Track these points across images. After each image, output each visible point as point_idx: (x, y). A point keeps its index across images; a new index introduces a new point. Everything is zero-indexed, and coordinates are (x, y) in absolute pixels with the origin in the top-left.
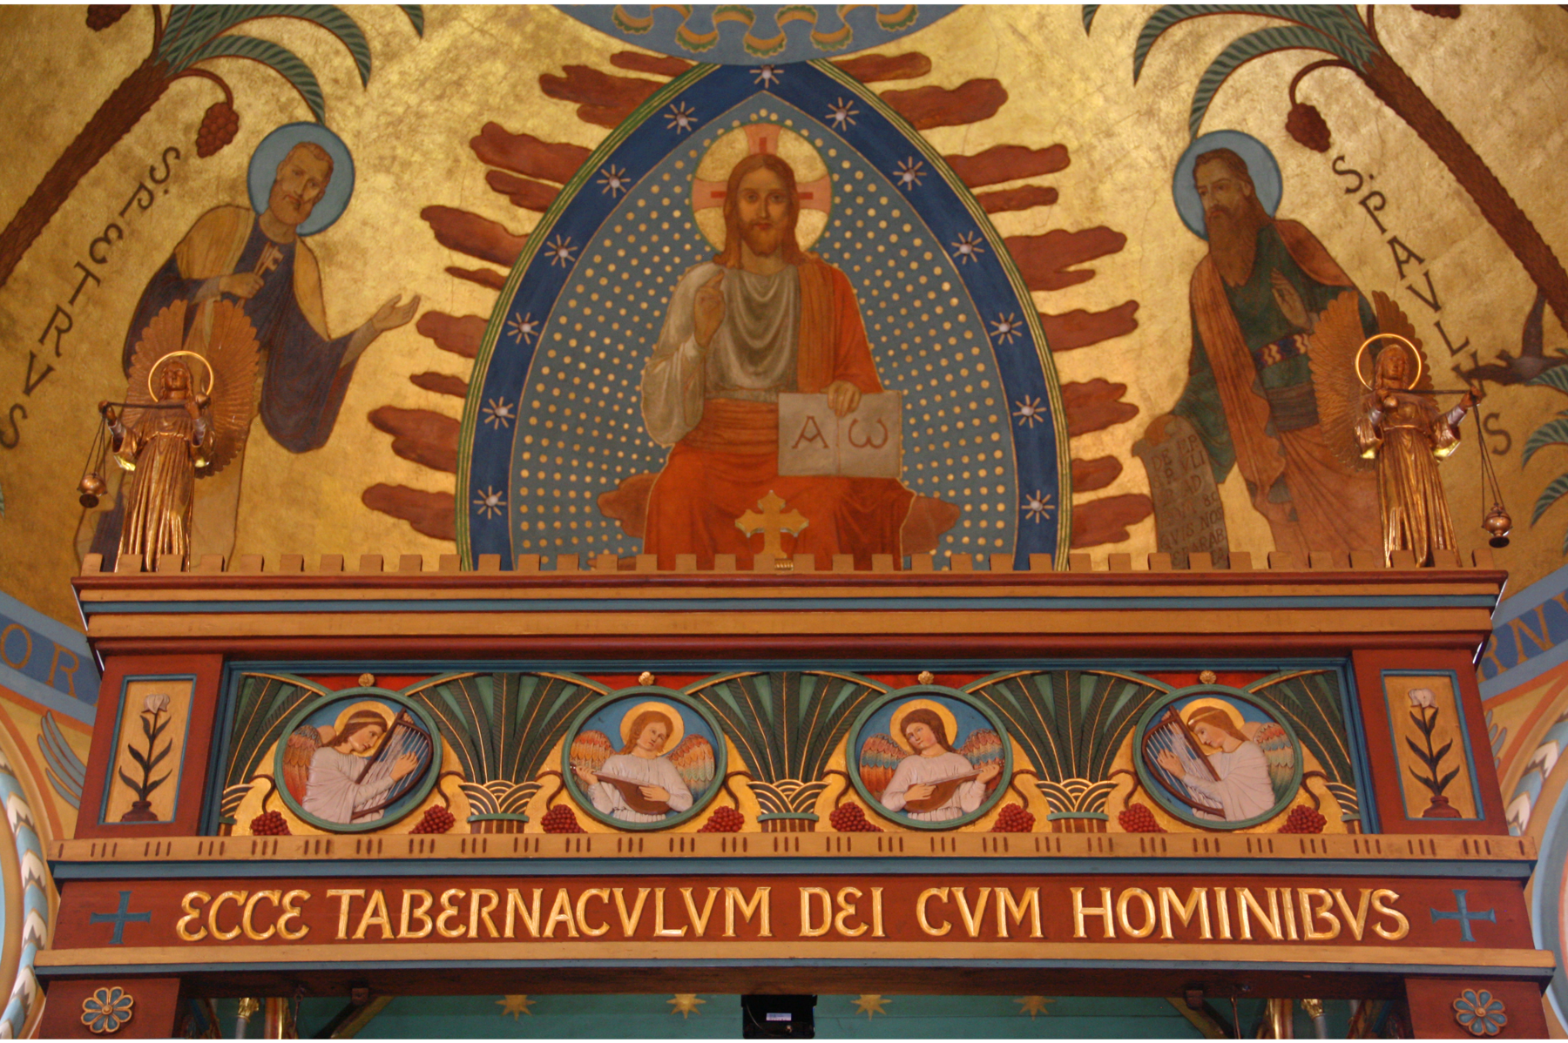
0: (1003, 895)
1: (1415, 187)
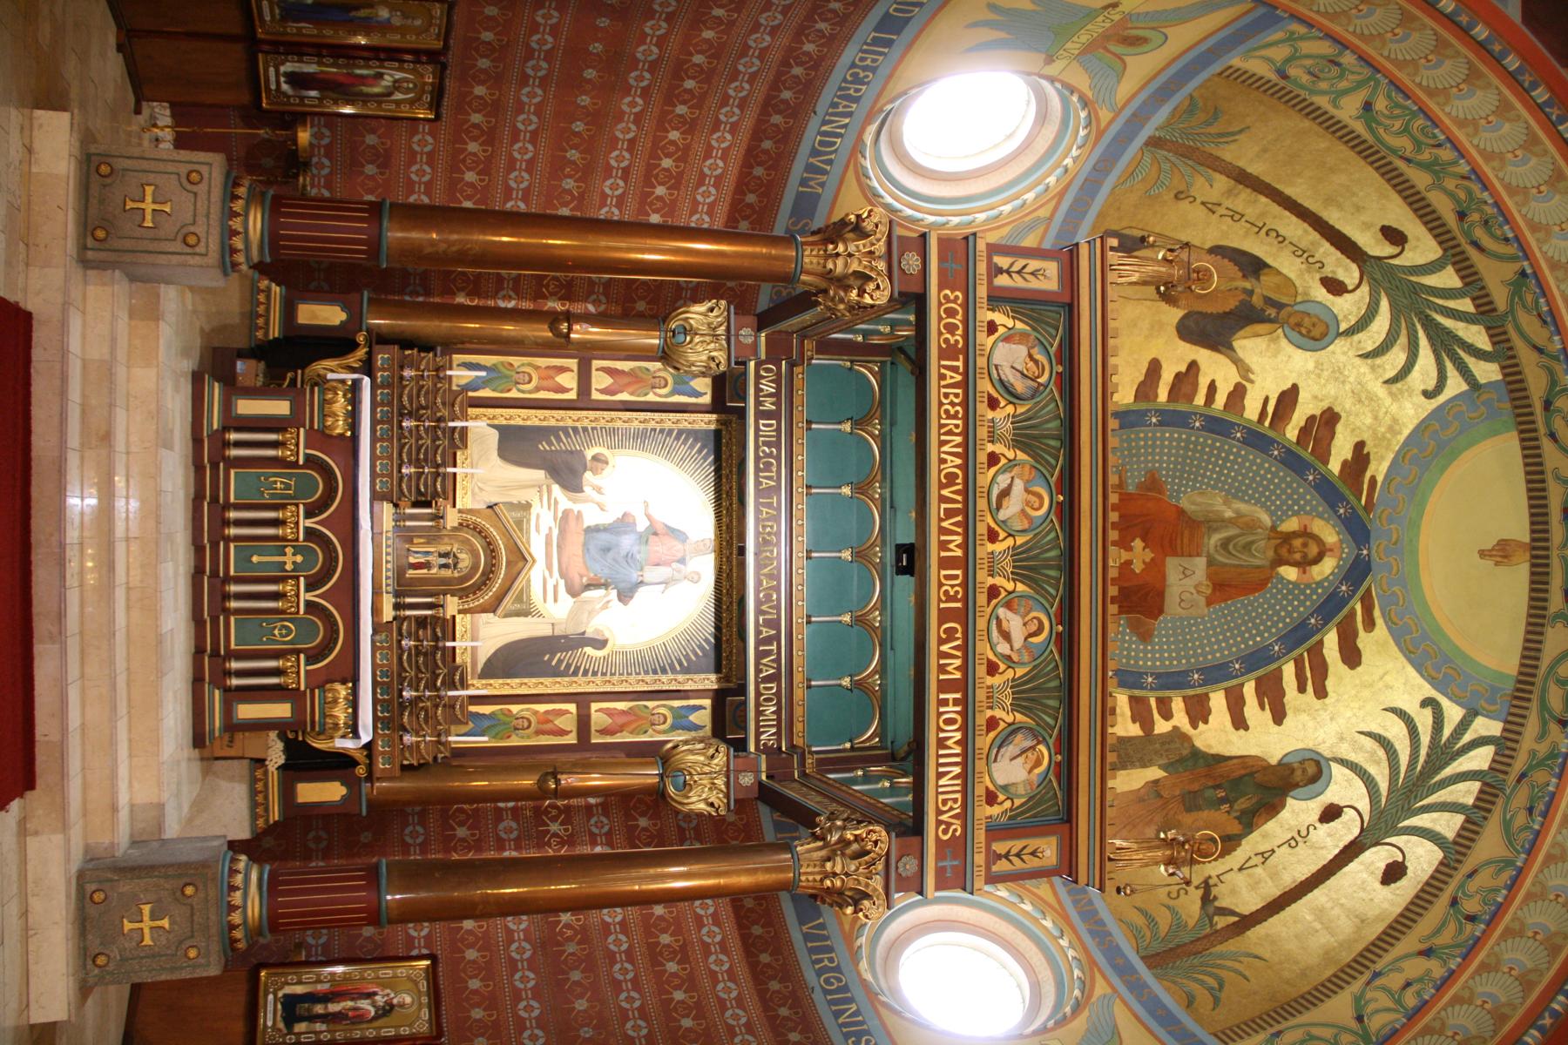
0: (958, 662)
1: (1299, 862)
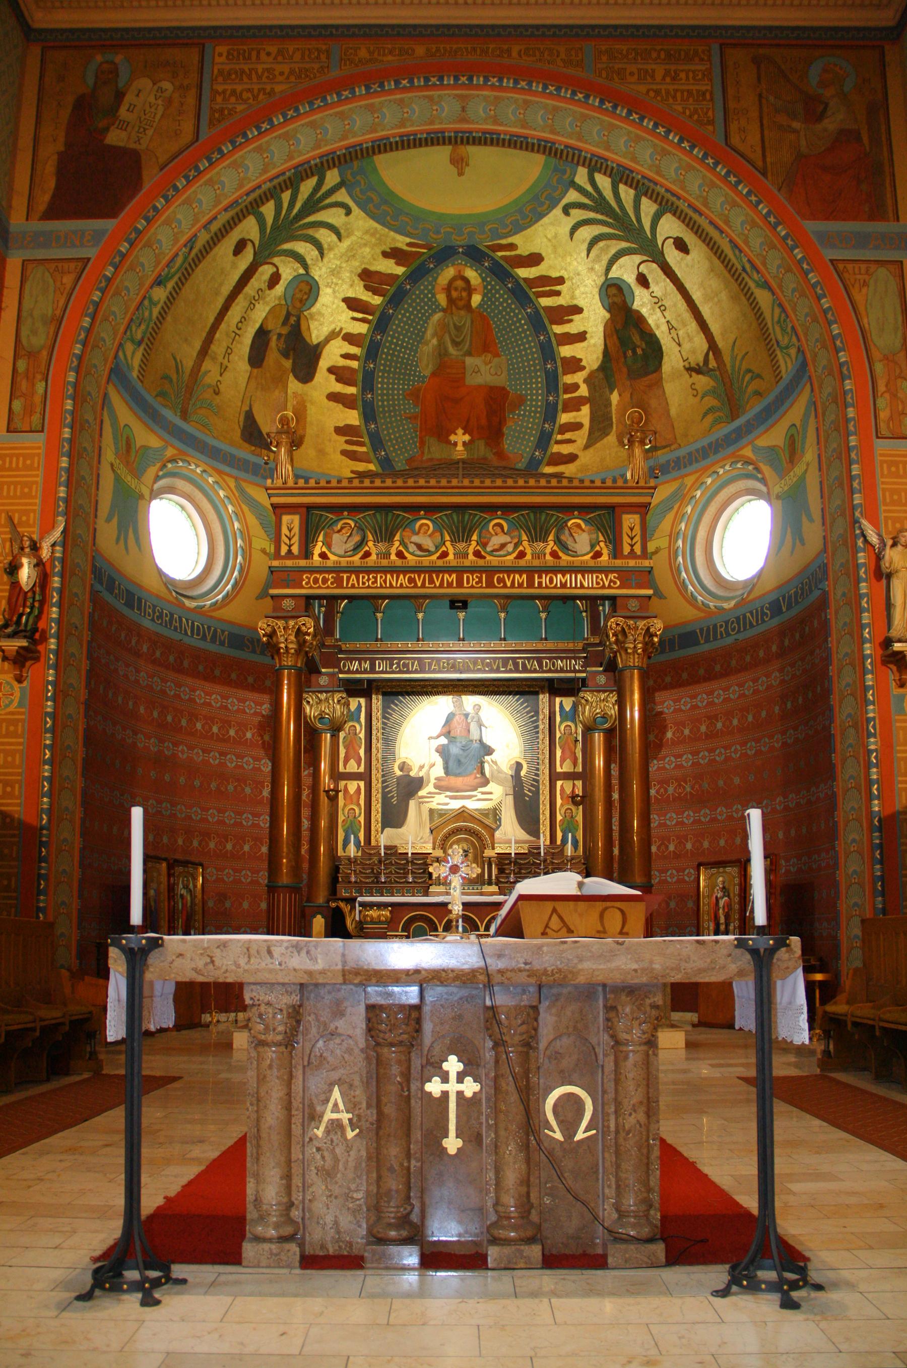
0: (517, 576)
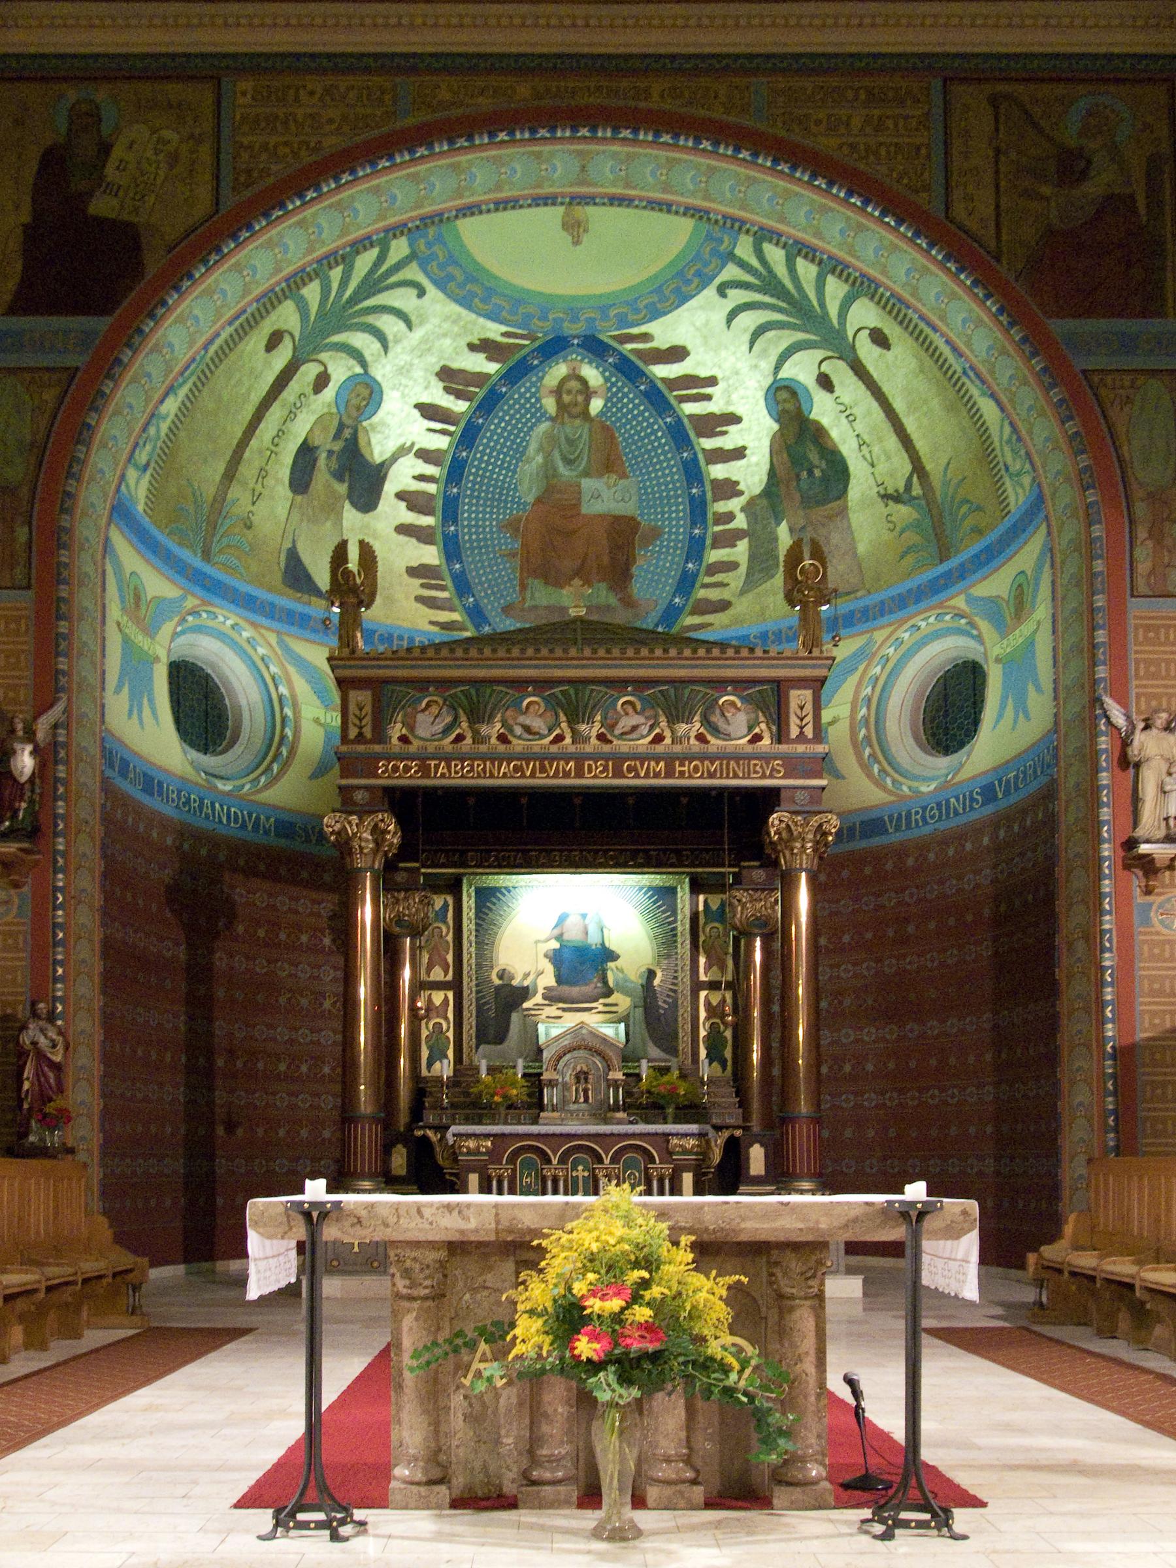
0: (653, 763)
